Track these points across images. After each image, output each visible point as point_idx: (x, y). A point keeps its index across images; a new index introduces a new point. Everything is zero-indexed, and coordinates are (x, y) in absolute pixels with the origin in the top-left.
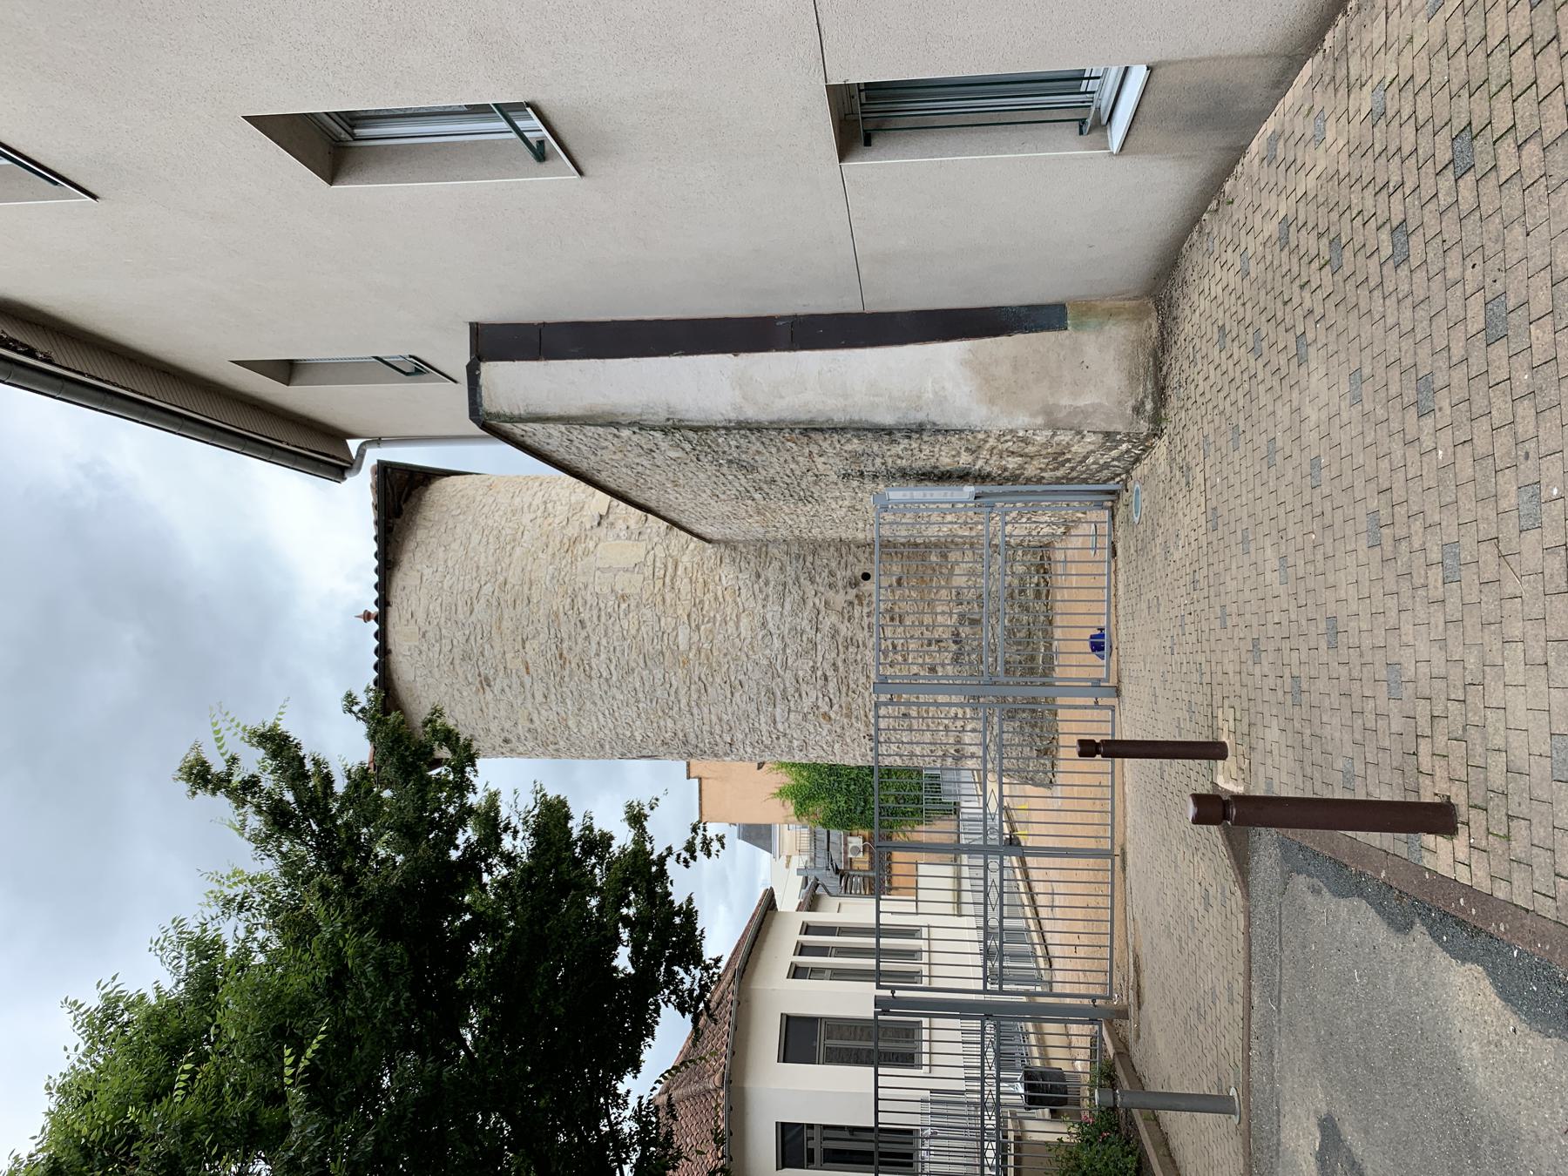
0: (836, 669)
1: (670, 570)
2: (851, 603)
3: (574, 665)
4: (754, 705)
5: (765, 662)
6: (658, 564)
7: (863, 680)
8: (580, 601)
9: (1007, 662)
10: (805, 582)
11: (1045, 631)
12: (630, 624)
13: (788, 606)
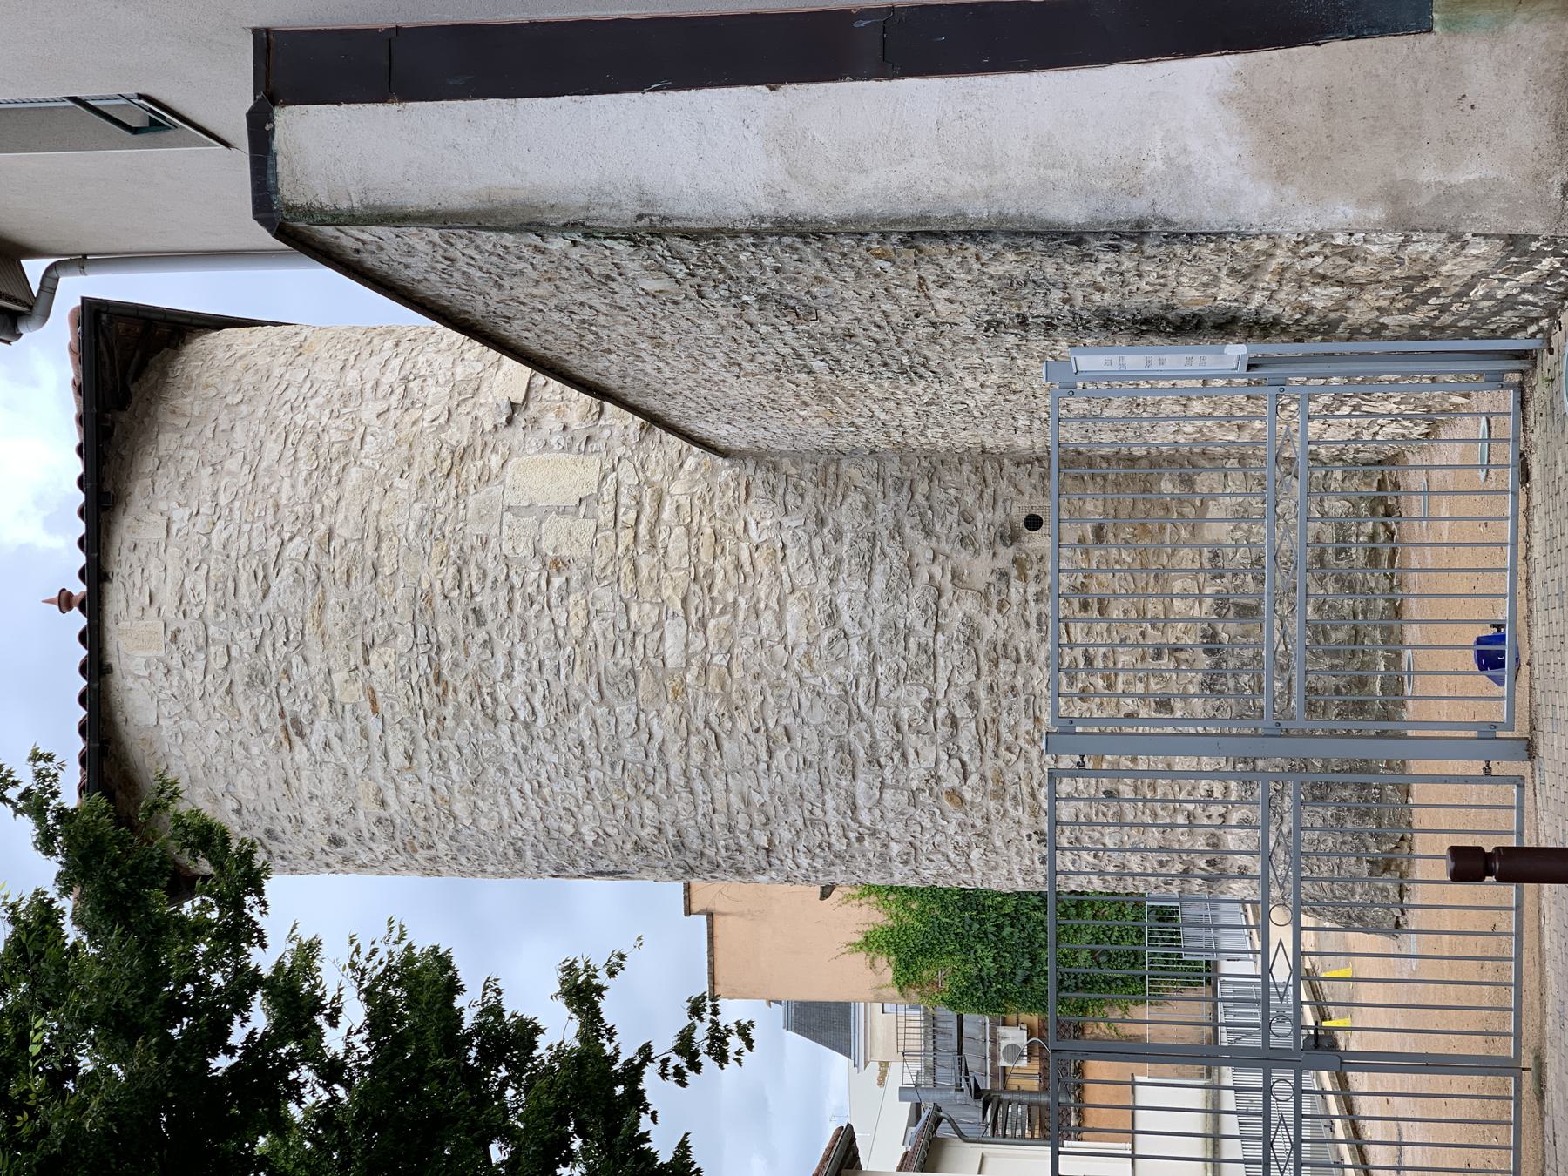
0: (974, 704)
2: (1003, 575)
3: (462, 696)
4: (812, 775)
5: (835, 691)
8: (474, 572)
9: (1311, 690)
12: (570, 616)
13: (879, 582)
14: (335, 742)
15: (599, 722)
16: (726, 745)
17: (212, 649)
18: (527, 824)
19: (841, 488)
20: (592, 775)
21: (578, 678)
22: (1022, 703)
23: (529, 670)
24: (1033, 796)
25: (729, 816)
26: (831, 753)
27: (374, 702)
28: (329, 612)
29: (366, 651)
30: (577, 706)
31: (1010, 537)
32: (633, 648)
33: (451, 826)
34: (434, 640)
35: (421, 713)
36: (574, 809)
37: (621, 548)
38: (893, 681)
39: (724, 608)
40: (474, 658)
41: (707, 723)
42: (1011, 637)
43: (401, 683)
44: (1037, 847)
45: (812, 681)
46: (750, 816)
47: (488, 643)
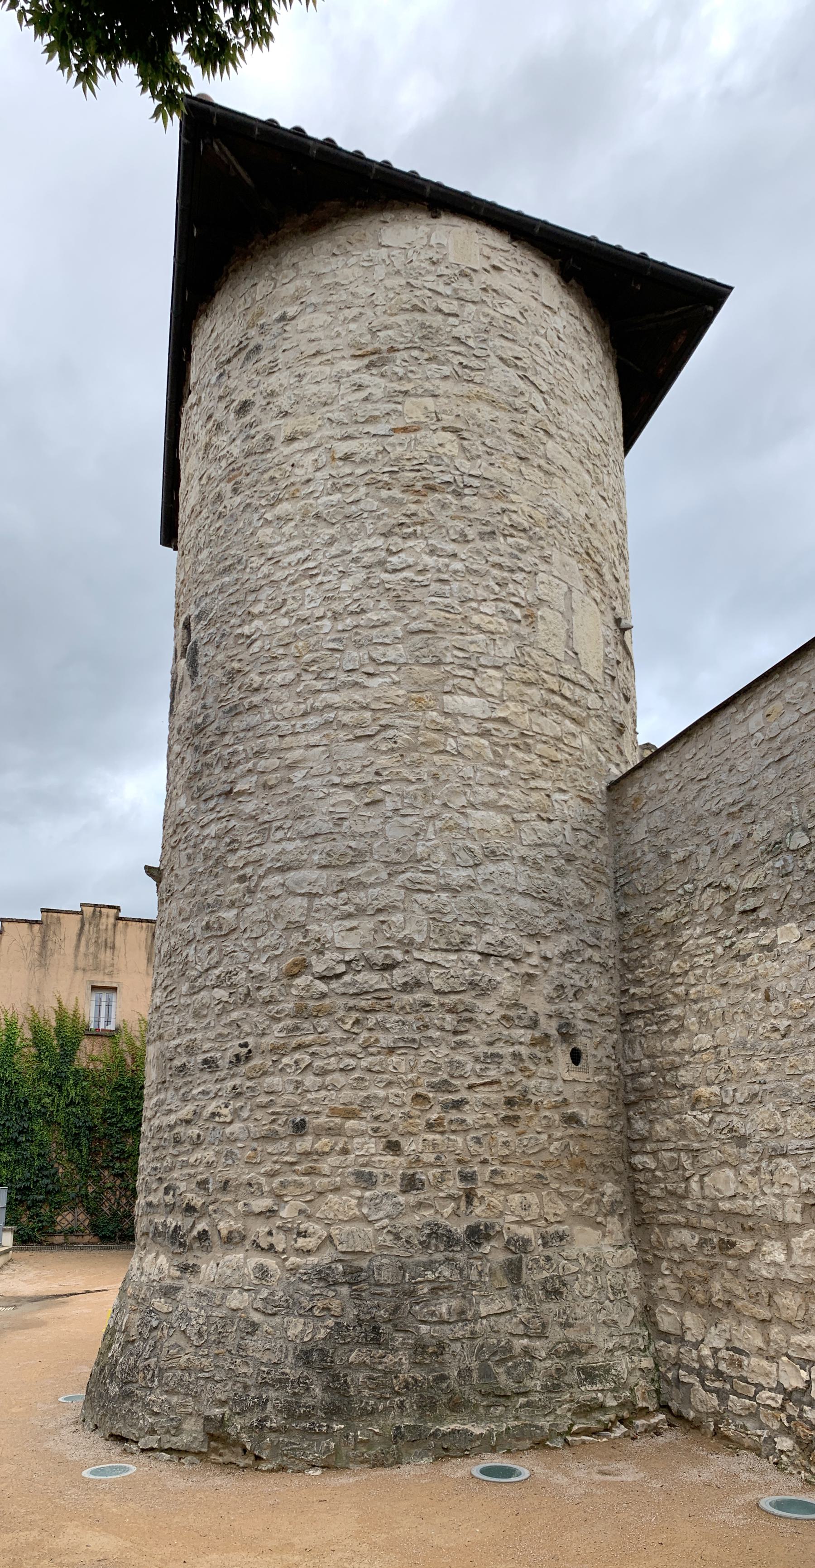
0: (406, 987)
1: (572, 709)
2: (534, 1024)
3: (413, 508)
4: (326, 827)
5: (420, 850)
6: (578, 691)
7: (386, 1040)
8: (525, 543)
9: (441, 1347)
10: (564, 941)
11: (520, 1433)
12: (488, 615)
13: (525, 903)
14: (363, 394)
15: (387, 629)
16: (361, 745)
17: (455, 302)
18: (265, 569)
19: (593, 883)
20: (327, 624)
21: (433, 614)
22: (411, 1036)
23: (439, 570)
24: (299, 1047)
25: (275, 750)
26: (353, 844)
27: (405, 430)
28: (489, 409)
29: (456, 431)
30: (403, 609)
31: (566, 1033)
32: (462, 666)
33: (263, 502)
34: (467, 491)
35: (396, 469)
36: (283, 610)
37: (545, 676)
38: (432, 907)
39: (500, 756)
40: (450, 523)
41: (385, 727)
42: (479, 1027)
43: (426, 455)
44: (229, 1054)
45: (431, 829)
46: (275, 770)
47: (464, 539)
